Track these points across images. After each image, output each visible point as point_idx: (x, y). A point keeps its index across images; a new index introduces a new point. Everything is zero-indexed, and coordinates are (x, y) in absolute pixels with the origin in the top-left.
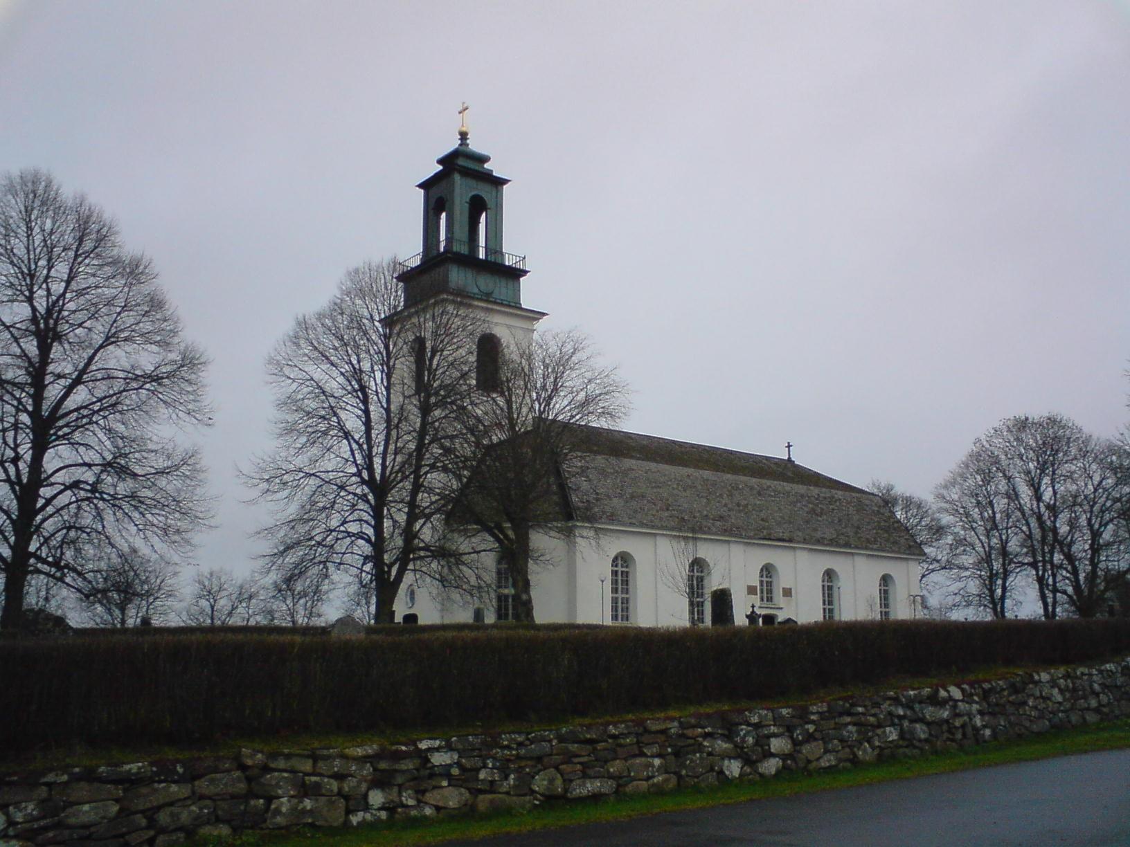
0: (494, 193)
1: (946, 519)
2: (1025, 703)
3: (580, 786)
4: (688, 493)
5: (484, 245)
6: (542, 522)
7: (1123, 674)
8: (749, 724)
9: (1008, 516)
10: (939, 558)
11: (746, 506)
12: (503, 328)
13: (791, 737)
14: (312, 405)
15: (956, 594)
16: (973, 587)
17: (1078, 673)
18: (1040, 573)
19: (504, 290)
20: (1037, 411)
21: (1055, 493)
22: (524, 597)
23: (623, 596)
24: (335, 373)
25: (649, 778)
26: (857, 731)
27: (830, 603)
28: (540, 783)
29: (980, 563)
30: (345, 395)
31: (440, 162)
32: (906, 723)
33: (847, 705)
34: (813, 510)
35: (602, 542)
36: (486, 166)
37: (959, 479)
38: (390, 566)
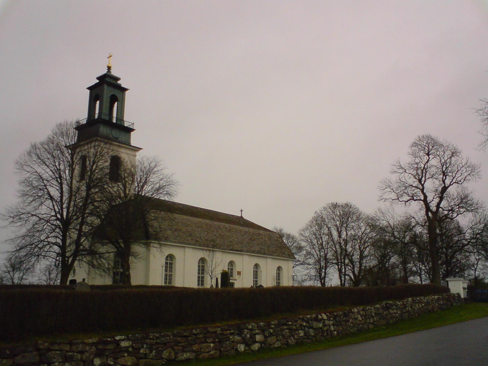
0: (121, 94)
1: (303, 244)
2: (348, 321)
3: (181, 356)
4: (199, 229)
5: (116, 117)
6: (137, 240)
7: (382, 309)
8: (248, 329)
9: (328, 243)
10: (300, 260)
11: (223, 236)
12: (124, 154)
13: (264, 335)
14: (35, 184)
15: (306, 275)
16: (313, 272)
17: (367, 309)
18: (340, 267)
19: (123, 137)
20: (341, 201)
21: (347, 234)
22: (127, 273)
23: (202, 275)
24: (48, 170)
25: (209, 352)
26: (289, 332)
27: (256, 278)
28: (165, 354)
29: (316, 262)
30: (52, 180)
31: (98, 78)
32: (307, 329)
33: (285, 321)
34: (251, 239)
35: (163, 250)
36: (119, 82)
37: (309, 227)
38: (68, 258)
